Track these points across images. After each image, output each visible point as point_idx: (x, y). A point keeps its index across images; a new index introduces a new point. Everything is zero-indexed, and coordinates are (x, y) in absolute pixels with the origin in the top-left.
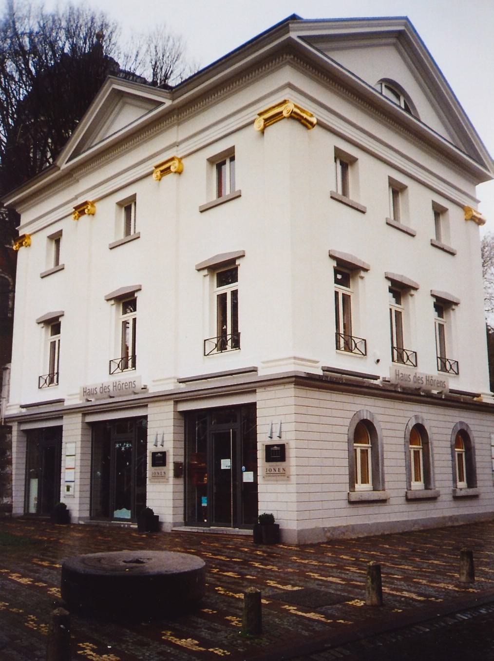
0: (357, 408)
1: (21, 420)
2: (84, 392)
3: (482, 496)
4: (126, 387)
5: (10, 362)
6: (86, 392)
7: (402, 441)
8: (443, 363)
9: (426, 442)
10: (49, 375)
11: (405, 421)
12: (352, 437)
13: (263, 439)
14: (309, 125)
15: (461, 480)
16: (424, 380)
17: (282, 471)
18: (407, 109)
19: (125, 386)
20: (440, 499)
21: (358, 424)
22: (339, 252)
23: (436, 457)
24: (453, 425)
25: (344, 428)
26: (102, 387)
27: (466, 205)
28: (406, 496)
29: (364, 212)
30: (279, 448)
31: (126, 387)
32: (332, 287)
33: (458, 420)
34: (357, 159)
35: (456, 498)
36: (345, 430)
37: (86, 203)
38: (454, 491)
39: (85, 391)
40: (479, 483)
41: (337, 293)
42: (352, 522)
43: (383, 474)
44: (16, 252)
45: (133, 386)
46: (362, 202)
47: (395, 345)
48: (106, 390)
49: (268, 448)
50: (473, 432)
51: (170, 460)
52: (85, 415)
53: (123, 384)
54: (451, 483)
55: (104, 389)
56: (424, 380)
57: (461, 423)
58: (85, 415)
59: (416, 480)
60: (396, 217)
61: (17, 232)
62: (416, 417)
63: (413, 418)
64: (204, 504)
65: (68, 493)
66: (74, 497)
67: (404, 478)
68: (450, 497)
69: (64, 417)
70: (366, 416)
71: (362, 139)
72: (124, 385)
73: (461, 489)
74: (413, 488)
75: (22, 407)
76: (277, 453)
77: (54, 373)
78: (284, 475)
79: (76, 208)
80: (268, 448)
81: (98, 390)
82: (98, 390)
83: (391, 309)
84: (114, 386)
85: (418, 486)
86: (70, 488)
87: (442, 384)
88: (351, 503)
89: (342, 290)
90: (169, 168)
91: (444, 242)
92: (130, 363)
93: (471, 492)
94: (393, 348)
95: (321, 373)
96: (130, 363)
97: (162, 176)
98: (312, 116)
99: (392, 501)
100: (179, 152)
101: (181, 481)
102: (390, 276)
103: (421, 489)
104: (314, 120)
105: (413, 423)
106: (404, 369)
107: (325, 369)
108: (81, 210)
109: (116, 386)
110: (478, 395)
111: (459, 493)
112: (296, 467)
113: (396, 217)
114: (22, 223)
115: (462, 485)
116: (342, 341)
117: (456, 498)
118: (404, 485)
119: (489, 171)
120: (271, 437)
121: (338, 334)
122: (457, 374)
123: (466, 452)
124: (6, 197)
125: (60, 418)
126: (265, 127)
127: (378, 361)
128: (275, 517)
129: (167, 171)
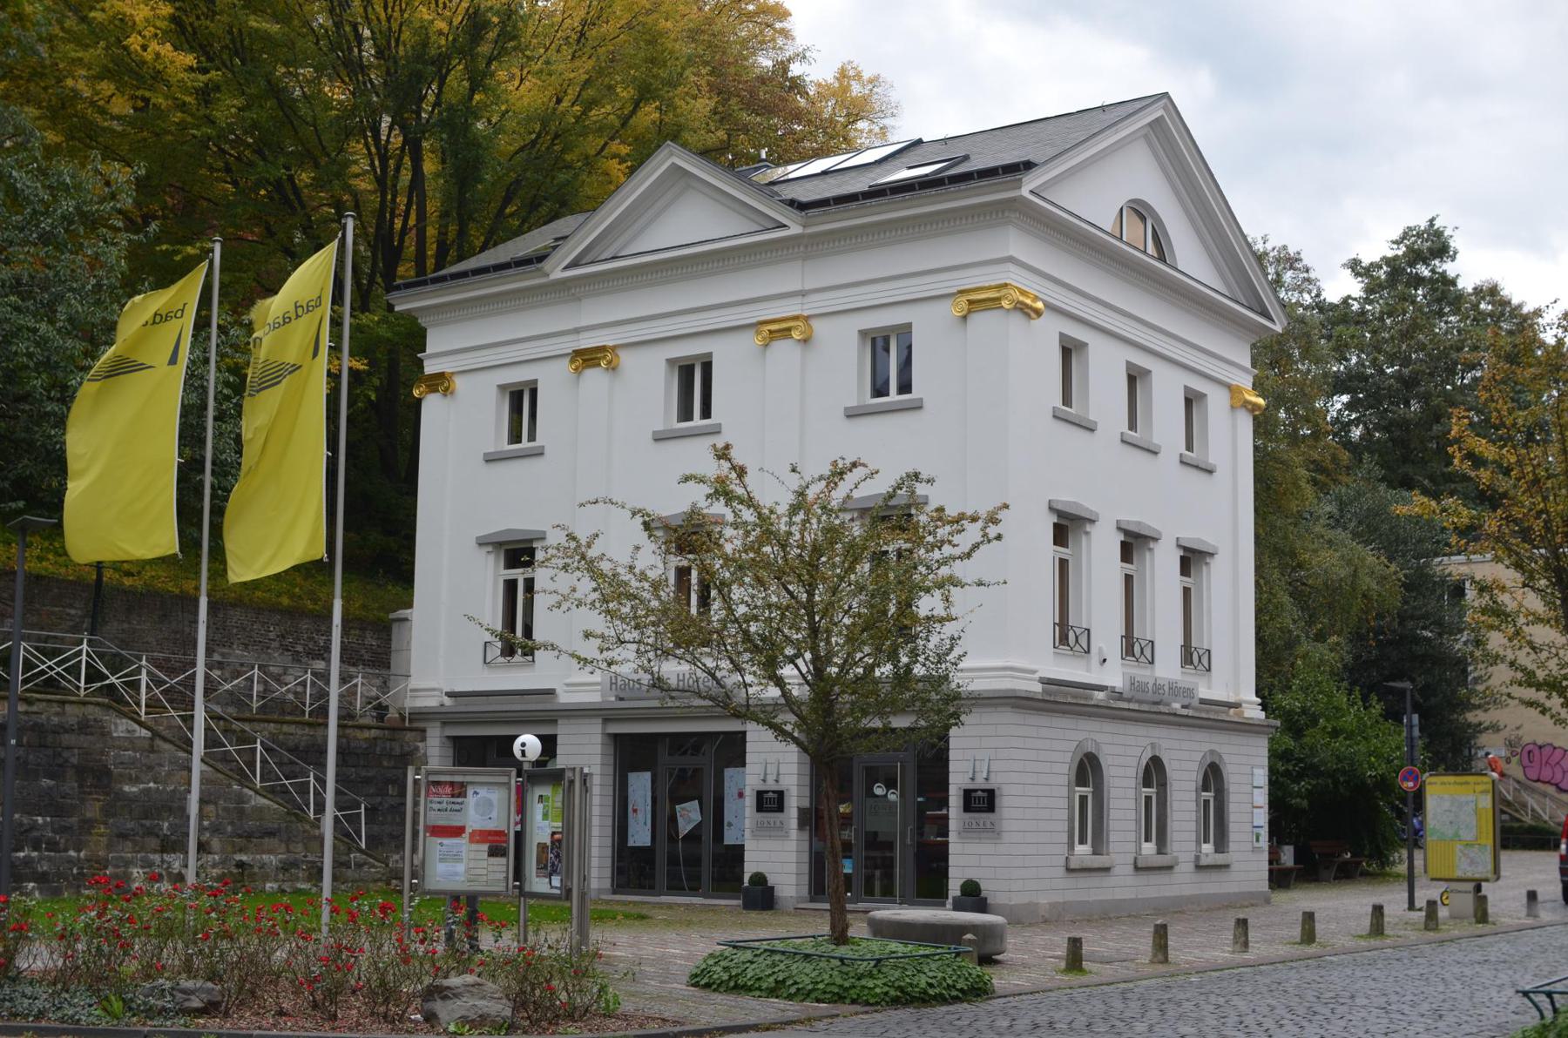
0: (1080, 736)
1: (444, 718)
3: (1234, 867)
5: (410, 605)
7: (1132, 783)
8: (1188, 655)
9: (1163, 785)
11: (1138, 752)
12: (1073, 778)
13: (958, 779)
14: (1033, 315)
15: (1082, 841)
16: (1166, 688)
17: (988, 826)
18: (1162, 258)
20: (1177, 869)
22: (1062, 502)
23: (1176, 806)
24: (1199, 756)
25: (1063, 768)
27: (1234, 383)
28: (1135, 862)
30: (985, 794)
33: (1207, 747)
34: (1086, 344)
35: (1199, 868)
36: (1065, 769)
37: (603, 349)
38: (1197, 858)
40: (1232, 846)
42: (1071, 896)
43: (1108, 831)
44: (419, 401)
49: (968, 795)
50: (1228, 766)
51: (793, 803)
52: (606, 721)
54: (1193, 846)
56: (1166, 688)
57: (1212, 752)
58: (606, 721)
59: (1146, 841)
61: (420, 364)
62: (1153, 745)
63: (1149, 748)
64: (848, 870)
67: (1064, 837)
68: (1191, 867)
69: (560, 722)
70: (1090, 748)
71: (1096, 314)
73: (1207, 855)
74: (1144, 852)
75: (450, 695)
76: (982, 801)
78: (994, 833)
79: (578, 353)
80: (968, 795)
85: (1149, 848)
87: (1189, 692)
90: (789, 329)
93: (1220, 859)
95: (1037, 688)
97: (772, 339)
98: (1036, 298)
99: (1116, 871)
100: (805, 307)
101: (806, 835)
102: (1123, 526)
104: (1040, 305)
105: (1148, 755)
106: (1142, 673)
107: (1046, 682)
108: (587, 358)
110: (1237, 705)
111: (1204, 862)
114: (431, 348)
115: (1208, 848)
117: (1199, 868)
118: (1132, 847)
119: (1273, 321)
120: (973, 779)
122: (1209, 670)
123: (1215, 798)
125: (554, 722)
126: (969, 311)
127: (1105, 660)
128: (983, 886)
129: (785, 333)
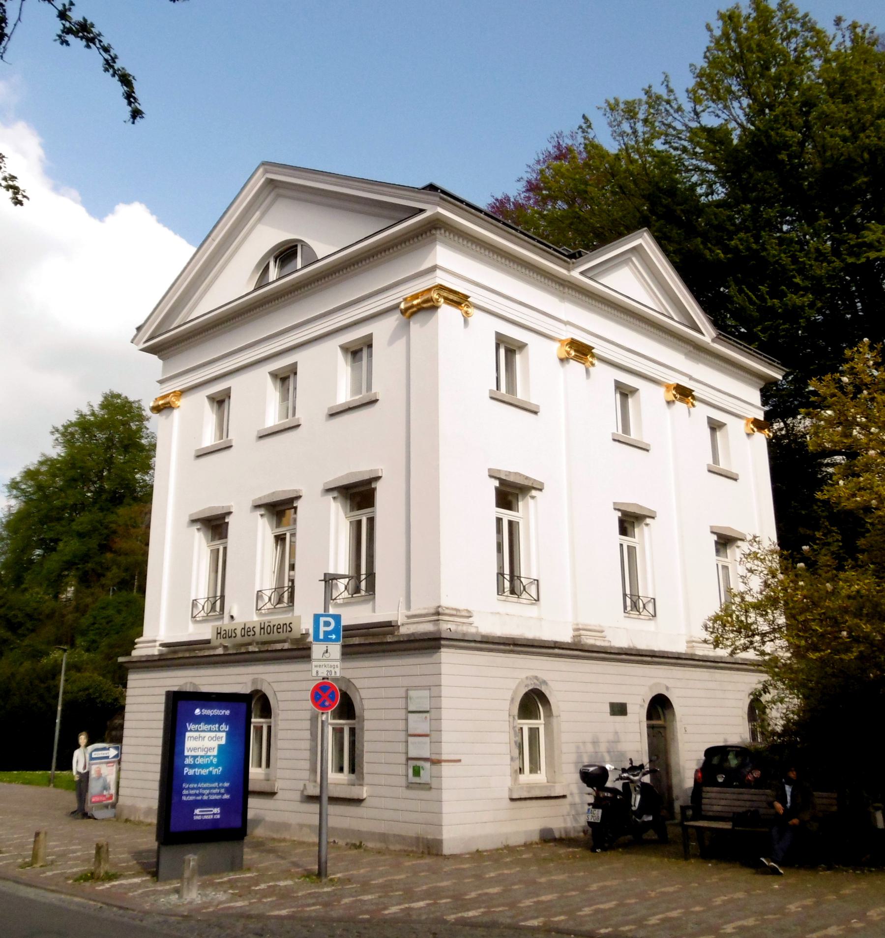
2: (218, 633)
4: (279, 630)
6: (220, 633)
10: (208, 598)
19: (278, 628)
21: (526, 694)
26: (244, 629)
29: (536, 413)
31: (279, 630)
32: (494, 510)
39: (262, 626)
41: (499, 521)
45: (289, 629)
46: (534, 400)
47: (628, 592)
48: (249, 633)
53: (274, 626)
55: (248, 632)
60: (626, 428)
65: (417, 780)
66: (430, 788)
72: (275, 627)
77: (215, 597)
81: (238, 632)
82: (238, 632)
83: (621, 545)
84: (261, 628)
86: (422, 772)
88: (512, 800)
89: (507, 515)
91: (723, 465)
92: (363, 585)
94: (625, 595)
96: (363, 585)
103: (172, 824)
109: (264, 628)
112: (444, 757)
113: (626, 428)
116: (507, 584)
121: (501, 574)
124: (403, 235)
